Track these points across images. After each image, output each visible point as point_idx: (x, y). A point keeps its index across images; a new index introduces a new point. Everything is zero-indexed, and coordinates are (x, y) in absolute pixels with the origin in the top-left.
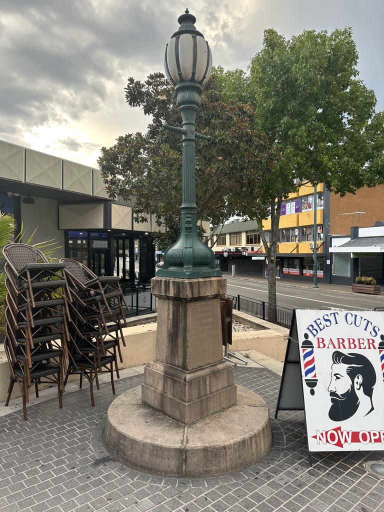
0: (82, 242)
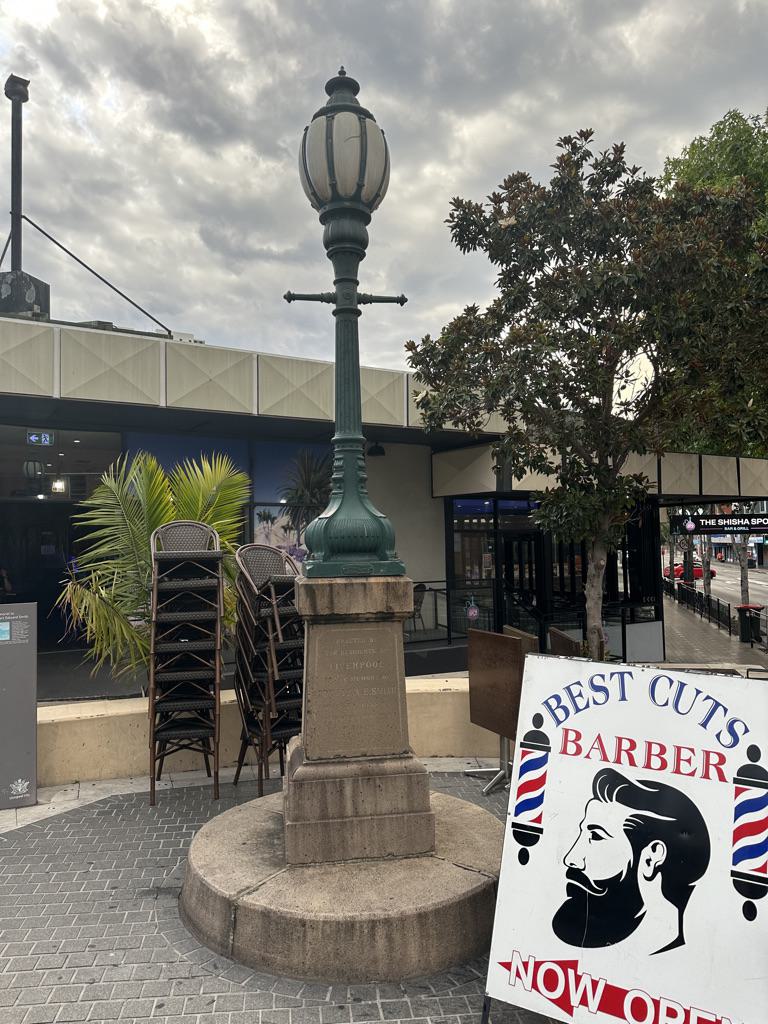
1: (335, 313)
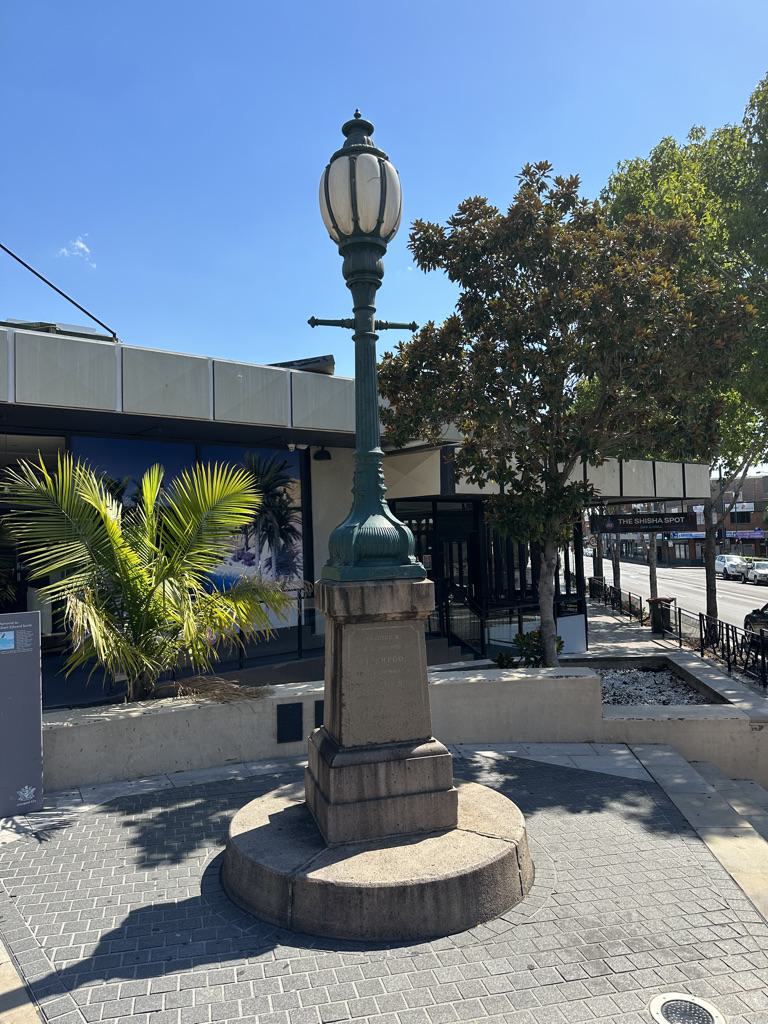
0: (427, 521)
1: (354, 338)
